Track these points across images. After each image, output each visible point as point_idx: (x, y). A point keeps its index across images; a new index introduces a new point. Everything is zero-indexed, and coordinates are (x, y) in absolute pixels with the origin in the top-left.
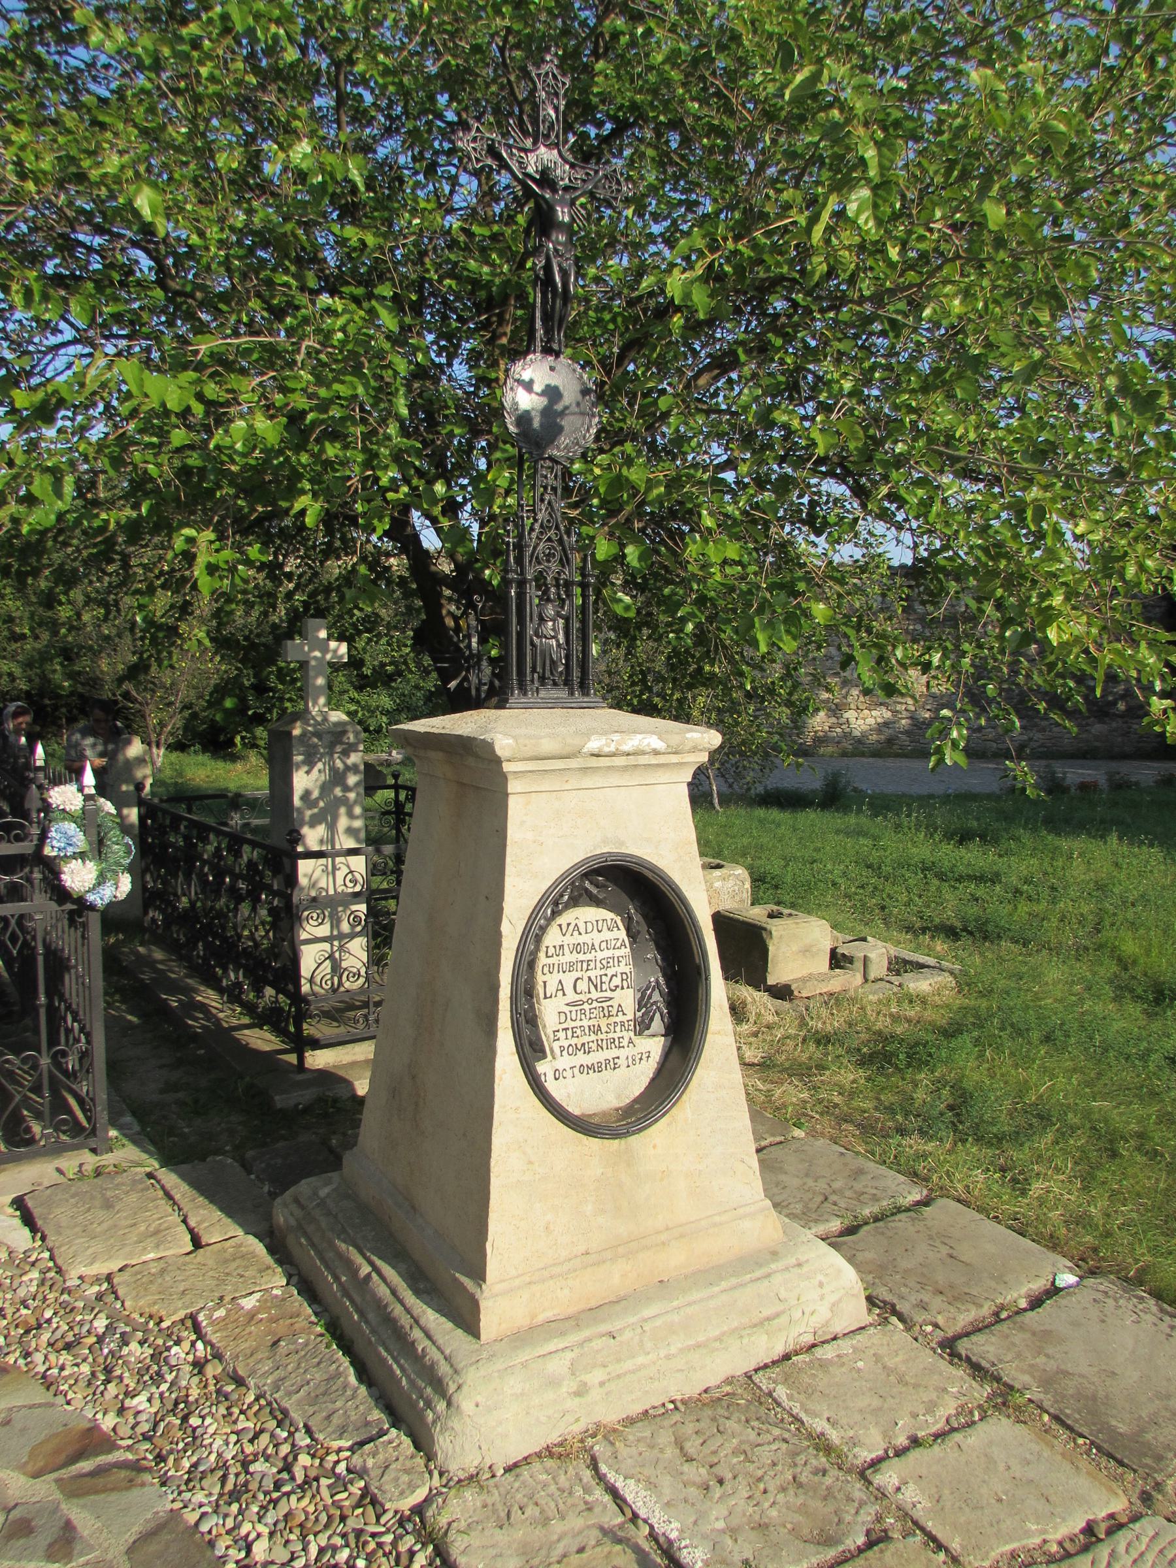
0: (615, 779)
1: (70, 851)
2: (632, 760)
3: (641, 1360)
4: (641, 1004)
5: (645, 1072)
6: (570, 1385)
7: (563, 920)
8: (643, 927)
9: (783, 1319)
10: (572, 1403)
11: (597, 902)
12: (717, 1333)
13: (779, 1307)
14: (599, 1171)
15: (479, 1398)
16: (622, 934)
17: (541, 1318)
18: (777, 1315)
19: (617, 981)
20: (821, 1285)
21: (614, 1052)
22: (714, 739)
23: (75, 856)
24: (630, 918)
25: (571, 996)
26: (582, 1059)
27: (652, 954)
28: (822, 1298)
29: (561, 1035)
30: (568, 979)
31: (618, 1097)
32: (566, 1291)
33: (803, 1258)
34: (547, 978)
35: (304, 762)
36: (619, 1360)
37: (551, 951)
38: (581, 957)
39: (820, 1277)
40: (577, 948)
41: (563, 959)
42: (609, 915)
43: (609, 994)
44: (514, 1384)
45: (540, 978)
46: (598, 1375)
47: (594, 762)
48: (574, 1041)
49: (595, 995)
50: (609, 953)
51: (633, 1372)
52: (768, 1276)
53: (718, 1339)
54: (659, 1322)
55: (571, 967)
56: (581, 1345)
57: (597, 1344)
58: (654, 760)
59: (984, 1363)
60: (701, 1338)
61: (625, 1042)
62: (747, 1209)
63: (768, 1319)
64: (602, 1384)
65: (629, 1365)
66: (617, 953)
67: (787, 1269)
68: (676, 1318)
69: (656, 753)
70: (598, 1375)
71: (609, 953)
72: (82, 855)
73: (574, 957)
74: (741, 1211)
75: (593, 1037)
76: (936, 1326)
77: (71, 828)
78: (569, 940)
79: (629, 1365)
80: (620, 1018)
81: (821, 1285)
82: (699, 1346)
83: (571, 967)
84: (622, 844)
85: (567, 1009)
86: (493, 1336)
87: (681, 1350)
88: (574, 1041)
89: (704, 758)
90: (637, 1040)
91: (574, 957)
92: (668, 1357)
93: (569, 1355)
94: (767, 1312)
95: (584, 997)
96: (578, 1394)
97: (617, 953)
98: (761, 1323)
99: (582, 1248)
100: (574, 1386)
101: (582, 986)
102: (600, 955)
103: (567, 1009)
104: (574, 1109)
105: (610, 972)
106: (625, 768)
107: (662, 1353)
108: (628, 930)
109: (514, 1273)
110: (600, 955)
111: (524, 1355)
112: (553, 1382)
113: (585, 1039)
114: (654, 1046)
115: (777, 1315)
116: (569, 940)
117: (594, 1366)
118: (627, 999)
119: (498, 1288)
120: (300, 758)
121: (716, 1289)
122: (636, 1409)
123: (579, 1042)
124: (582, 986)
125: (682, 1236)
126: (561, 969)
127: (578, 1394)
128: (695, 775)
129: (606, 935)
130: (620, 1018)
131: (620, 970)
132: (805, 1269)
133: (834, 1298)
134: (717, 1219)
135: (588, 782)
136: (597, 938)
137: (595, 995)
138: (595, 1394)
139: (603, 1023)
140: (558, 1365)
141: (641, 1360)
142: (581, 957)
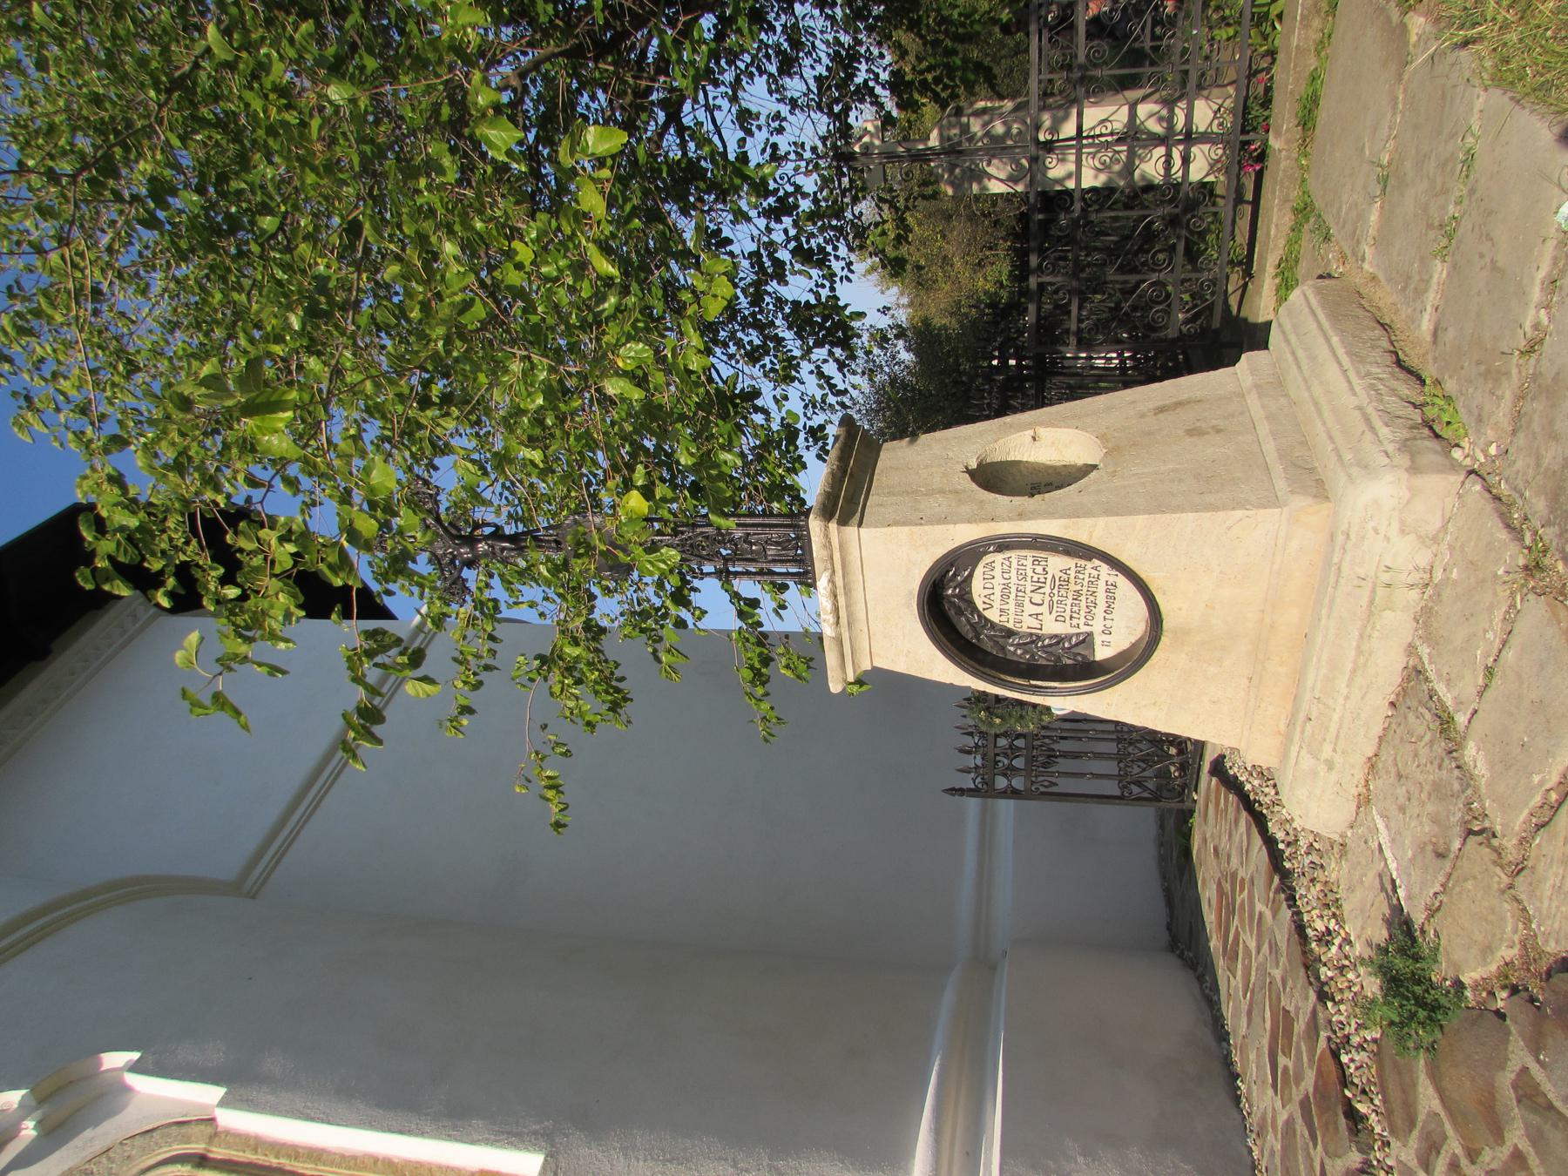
0: (858, 594)
2: (840, 591)
3: (1336, 717)
6: (1322, 768)
7: (980, 606)
9: (1380, 592)
10: (1334, 776)
13: (1368, 586)
17: (1282, 727)
18: (1373, 591)
19: (1039, 569)
20: (1376, 531)
21: (1102, 584)
25: (1044, 609)
28: (1387, 539)
29: (1075, 622)
35: (980, 182)
36: (1327, 729)
38: (1013, 596)
39: (1370, 525)
40: (1005, 597)
42: (979, 570)
43: (1049, 577)
45: (1025, 629)
48: (1083, 613)
49: (1047, 590)
50: (1014, 572)
51: (1340, 728)
53: (1359, 651)
54: (1319, 685)
55: (1019, 605)
58: (839, 573)
60: (1349, 666)
61: (1095, 573)
63: (1371, 602)
64: (1334, 750)
65: (1333, 728)
66: (1014, 565)
71: (1014, 572)
73: (1012, 601)
75: (1083, 598)
78: (997, 604)
79: (1333, 728)
80: (1072, 573)
81: (1376, 531)
82: (1354, 671)
83: (1019, 605)
84: (910, 593)
85: (1054, 614)
88: (1083, 613)
91: (1012, 601)
93: (1303, 752)
94: (1364, 601)
95: (1047, 599)
97: (1014, 565)
101: (1037, 598)
102: (1014, 580)
105: (1030, 573)
107: (1341, 700)
110: (1014, 580)
112: (1314, 774)
113: (1083, 604)
115: (1373, 591)
116: (997, 604)
120: (975, 187)
121: (1323, 622)
124: (1037, 598)
129: (997, 572)
130: (1072, 573)
133: (1395, 526)
135: (861, 614)
136: (999, 580)
137: (1047, 590)
138: (1338, 759)
139: (1073, 587)
140: (1307, 762)
141: (1336, 717)
142: (1013, 596)
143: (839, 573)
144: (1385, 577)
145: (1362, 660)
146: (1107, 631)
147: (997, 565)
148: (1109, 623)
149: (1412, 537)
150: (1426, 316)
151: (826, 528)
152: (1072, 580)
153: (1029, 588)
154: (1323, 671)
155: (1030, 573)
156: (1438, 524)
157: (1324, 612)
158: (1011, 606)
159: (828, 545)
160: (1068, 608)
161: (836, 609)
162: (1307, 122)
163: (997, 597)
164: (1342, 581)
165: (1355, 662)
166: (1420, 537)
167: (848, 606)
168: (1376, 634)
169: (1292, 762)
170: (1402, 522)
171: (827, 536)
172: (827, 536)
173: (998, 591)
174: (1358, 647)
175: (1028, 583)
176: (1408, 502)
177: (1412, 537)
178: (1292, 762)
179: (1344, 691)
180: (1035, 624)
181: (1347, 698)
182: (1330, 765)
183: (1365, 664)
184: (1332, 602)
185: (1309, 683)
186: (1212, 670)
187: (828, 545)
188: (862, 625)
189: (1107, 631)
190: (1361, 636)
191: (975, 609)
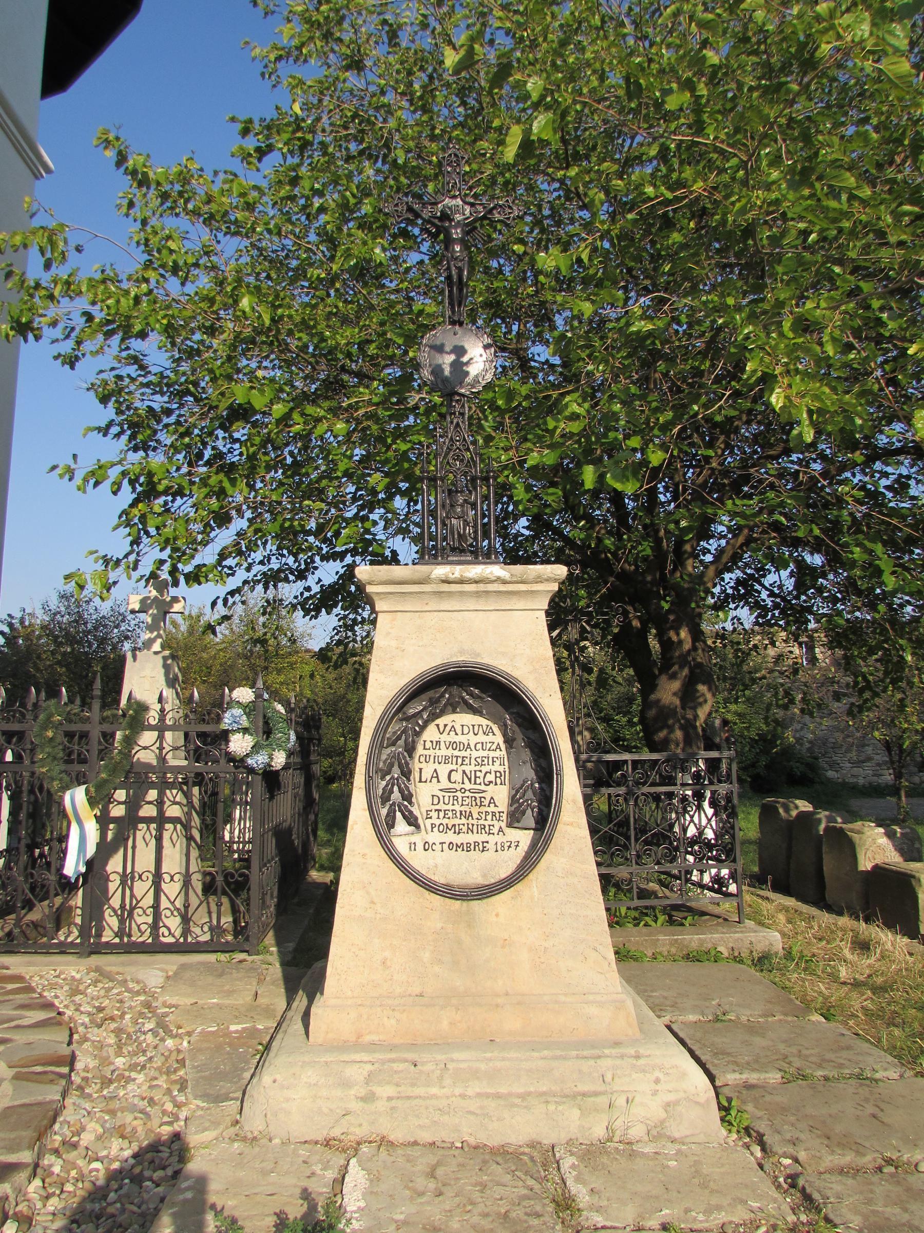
0: (471, 604)
1: (235, 726)
2: (481, 587)
3: (434, 1090)
4: (513, 800)
5: (514, 858)
7: (441, 721)
8: (519, 736)
9: (603, 1100)
10: (355, 1105)
11: (475, 711)
12: (521, 1090)
13: (601, 1088)
14: (439, 925)
15: (278, 1077)
16: (499, 739)
17: (368, 1038)
18: (596, 1094)
19: (490, 777)
20: (657, 1081)
21: (484, 837)
22: (561, 571)
23: (238, 730)
24: (505, 725)
25: (445, 784)
26: (450, 837)
27: (527, 755)
28: (655, 1093)
29: (434, 814)
30: (443, 771)
31: (484, 876)
32: (393, 1022)
33: (642, 1051)
34: (423, 765)
36: (413, 1085)
37: (428, 745)
38: (456, 753)
39: (657, 1074)
40: (453, 745)
41: (439, 753)
42: (484, 722)
43: (483, 787)
44: (310, 1075)
46: (390, 1090)
47: (446, 588)
48: (445, 821)
49: (468, 786)
50: (485, 753)
52: (599, 1057)
53: (523, 1096)
55: (447, 760)
56: (383, 1062)
57: (402, 1066)
58: (502, 588)
59: (816, 1196)
60: (503, 1090)
61: (495, 830)
62: (598, 998)
63: (584, 1095)
64: (390, 1099)
65: (420, 1091)
66: (492, 754)
67: (622, 1057)
68: (483, 1066)
69: (505, 582)
70: (390, 1090)
72: (245, 731)
73: (450, 752)
74: (591, 997)
75: (464, 821)
76: (796, 1160)
77: (238, 712)
79: (420, 1091)
80: (492, 808)
81: (657, 1081)
82: (498, 1096)
83: (447, 760)
84: (478, 655)
85: (440, 794)
86: (320, 1041)
87: (479, 1095)
88: (445, 821)
89: (555, 587)
90: (508, 831)
91: (450, 752)
92: (463, 1096)
93: (369, 1067)
94: (582, 1088)
95: (458, 787)
96: (364, 1099)
98: (574, 1096)
99: (417, 990)
100: (363, 1092)
101: (457, 777)
102: (475, 754)
103: (440, 794)
104: (439, 878)
105: (485, 769)
106: (478, 594)
107: (457, 1091)
108: (505, 735)
109: (349, 993)
110: (475, 754)
111: (329, 1058)
112: (346, 1084)
113: (457, 821)
114: (525, 838)
115: (596, 1094)
117: (389, 1083)
118: (501, 795)
119: (333, 1002)
121: (536, 1054)
122: (426, 1136)
123: (450, 823)
124: (457, 777)
125: (519, 1003)
126: (436, 760)
127: (364, 1099)
128: (552, 600)
129: (481, 738)
130: (492, 808)
131: (494, 768)
132: (641, 1062)
133: (671, 1097)
134: (562, 998)
135: (445, 605)
136: (473, 740)
137: (468, 786)
138: (381, 1105)
140: (357, 1073)
142: (456, 753)
143: (502, 588)
144: (621, 1101)
145: (518, 1101)
146: (427, 846)
147: (490, 738)
148: (438, 847)
149: (663, 1115)
150: (737, 1076)
151: (555, 580)
152: (483, 809)
153: (467, 769)
154: (483, 1066)
155: (485, 769)
156: (677, 1135)
157: (546, 1052)
158: (444, 752)
159: (539, 580)
160: (450, 807)
161: (461, 582)
162: (692, 957)
163: (452, 738)
164: (592, 1062)
165: (510, 1094)
166: (662, 1122)
167: (462, 593)
168: (552, 1107)
169: (345, 1057)
170: (677, 1103)
171: (548, 580)
172: (548, 580)
173: (463, 739)
174: (529, 1094)
175: (473, 768)
176: (697, 1103)
177: (663, 1115)
178: (345, 1057)
179: (470, 1092)
180: (426, 775)
181: (463, 1096)
182: (369, 1098)
183: (514, 1105)
184: (564, 1058)
185: (456, 1055)
186: (426, 956)
187: (539, 580)
188: (433, 606)
189: (427, 846)
190: (544, 1094)
191: (434, 717)
